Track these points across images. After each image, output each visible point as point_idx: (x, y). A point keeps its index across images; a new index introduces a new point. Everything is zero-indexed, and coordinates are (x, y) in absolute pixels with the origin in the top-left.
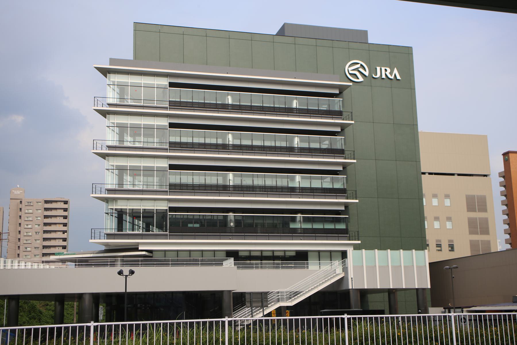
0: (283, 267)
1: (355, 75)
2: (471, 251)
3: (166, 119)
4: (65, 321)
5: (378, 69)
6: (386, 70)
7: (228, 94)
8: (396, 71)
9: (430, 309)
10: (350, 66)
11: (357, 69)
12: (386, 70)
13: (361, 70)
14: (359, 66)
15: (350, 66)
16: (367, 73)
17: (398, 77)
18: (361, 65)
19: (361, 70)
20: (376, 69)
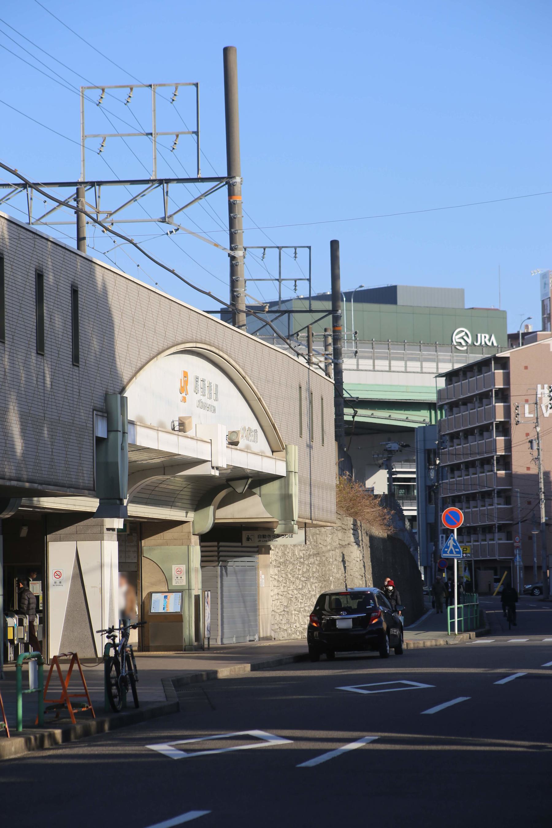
0: (426, 494)
1: (460, 343)
2: (143, 671)
3: (191, 549)
4: (538, 340)
5: (479, 335)
6: (485, 337)
7: (16, 753)
8: (493, 338)
9: (423, 567)
10: (457, 335)
11: (462, 338)
12: (485, 337)
13: (465, 338)
14: (463, 334)
15: (457, 335)
16: (470, 341)
17: (495, 344)
18: (466, 333)
19: (465, 338)
20: (477, 335)
